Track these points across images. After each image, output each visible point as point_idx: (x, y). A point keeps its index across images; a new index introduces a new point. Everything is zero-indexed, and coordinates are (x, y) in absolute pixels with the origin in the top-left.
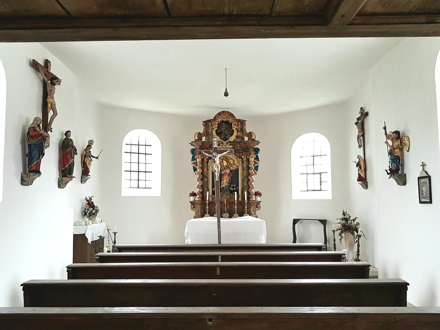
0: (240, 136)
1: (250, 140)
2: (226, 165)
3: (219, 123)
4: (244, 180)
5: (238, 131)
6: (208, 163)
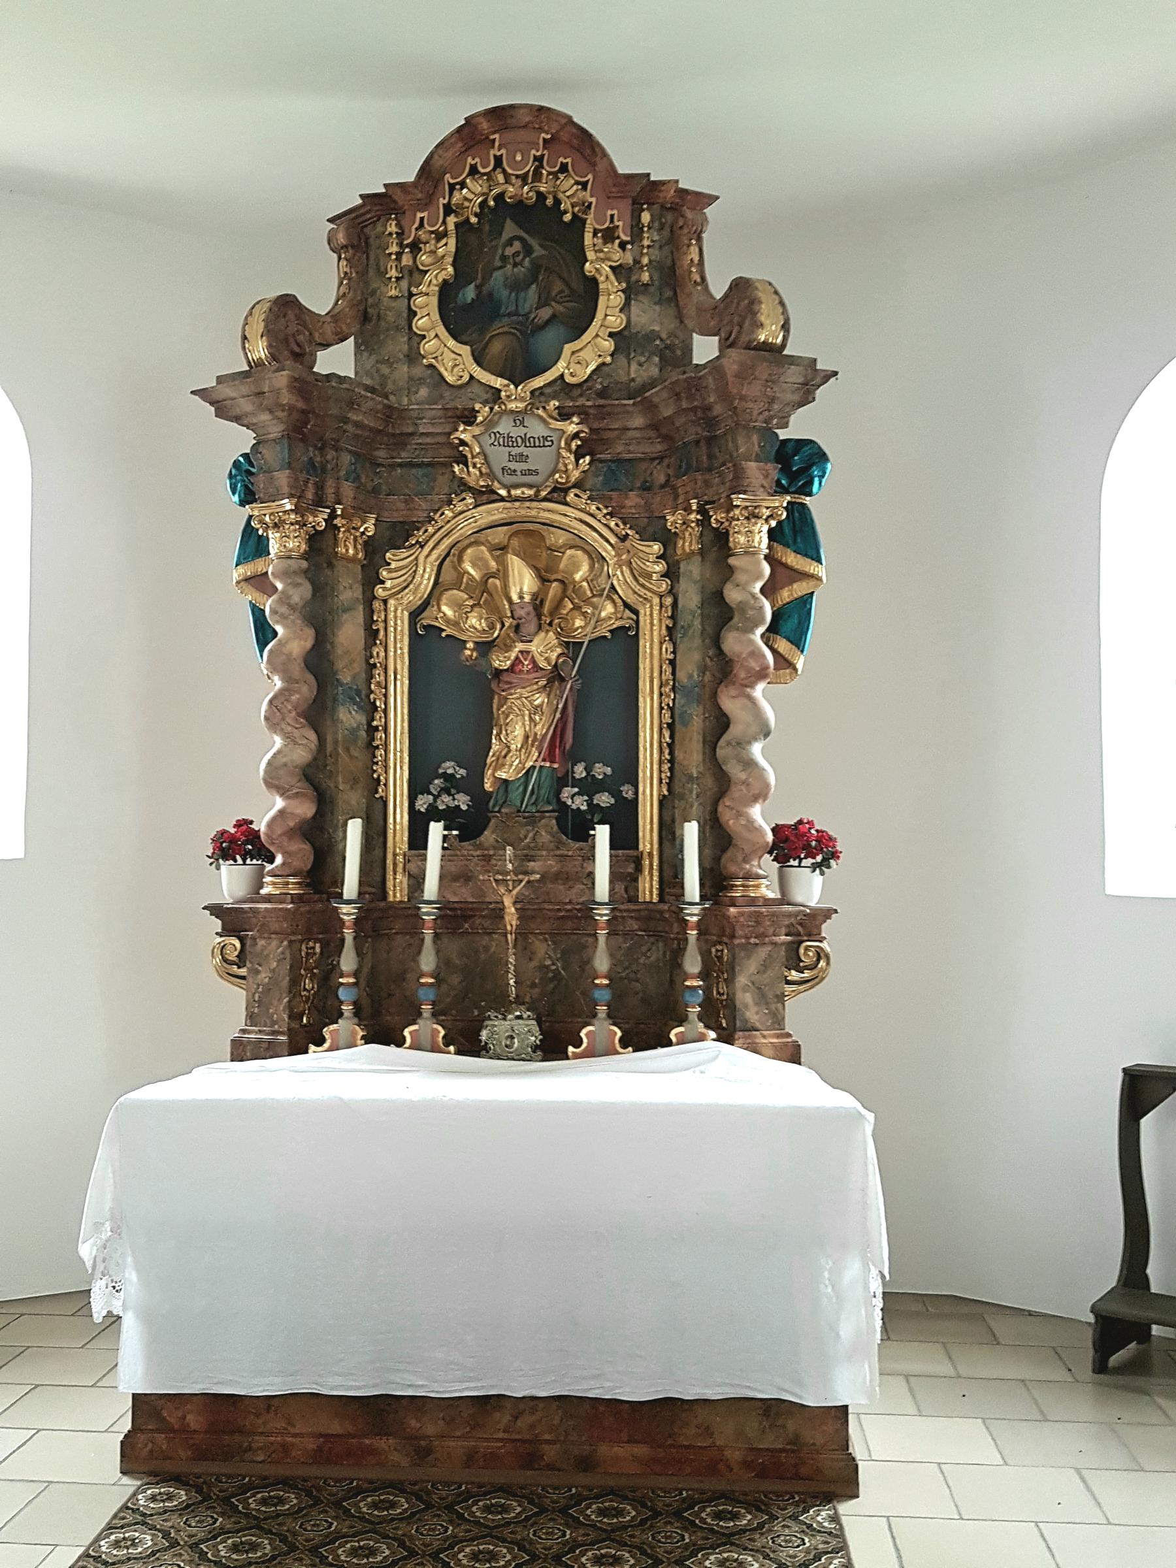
0: (651, 336)
1: (733, 353)
2: (527, 598)
3: (474, 220)
4: (678, 727)
5: (630, 293)
6: (371, 580)
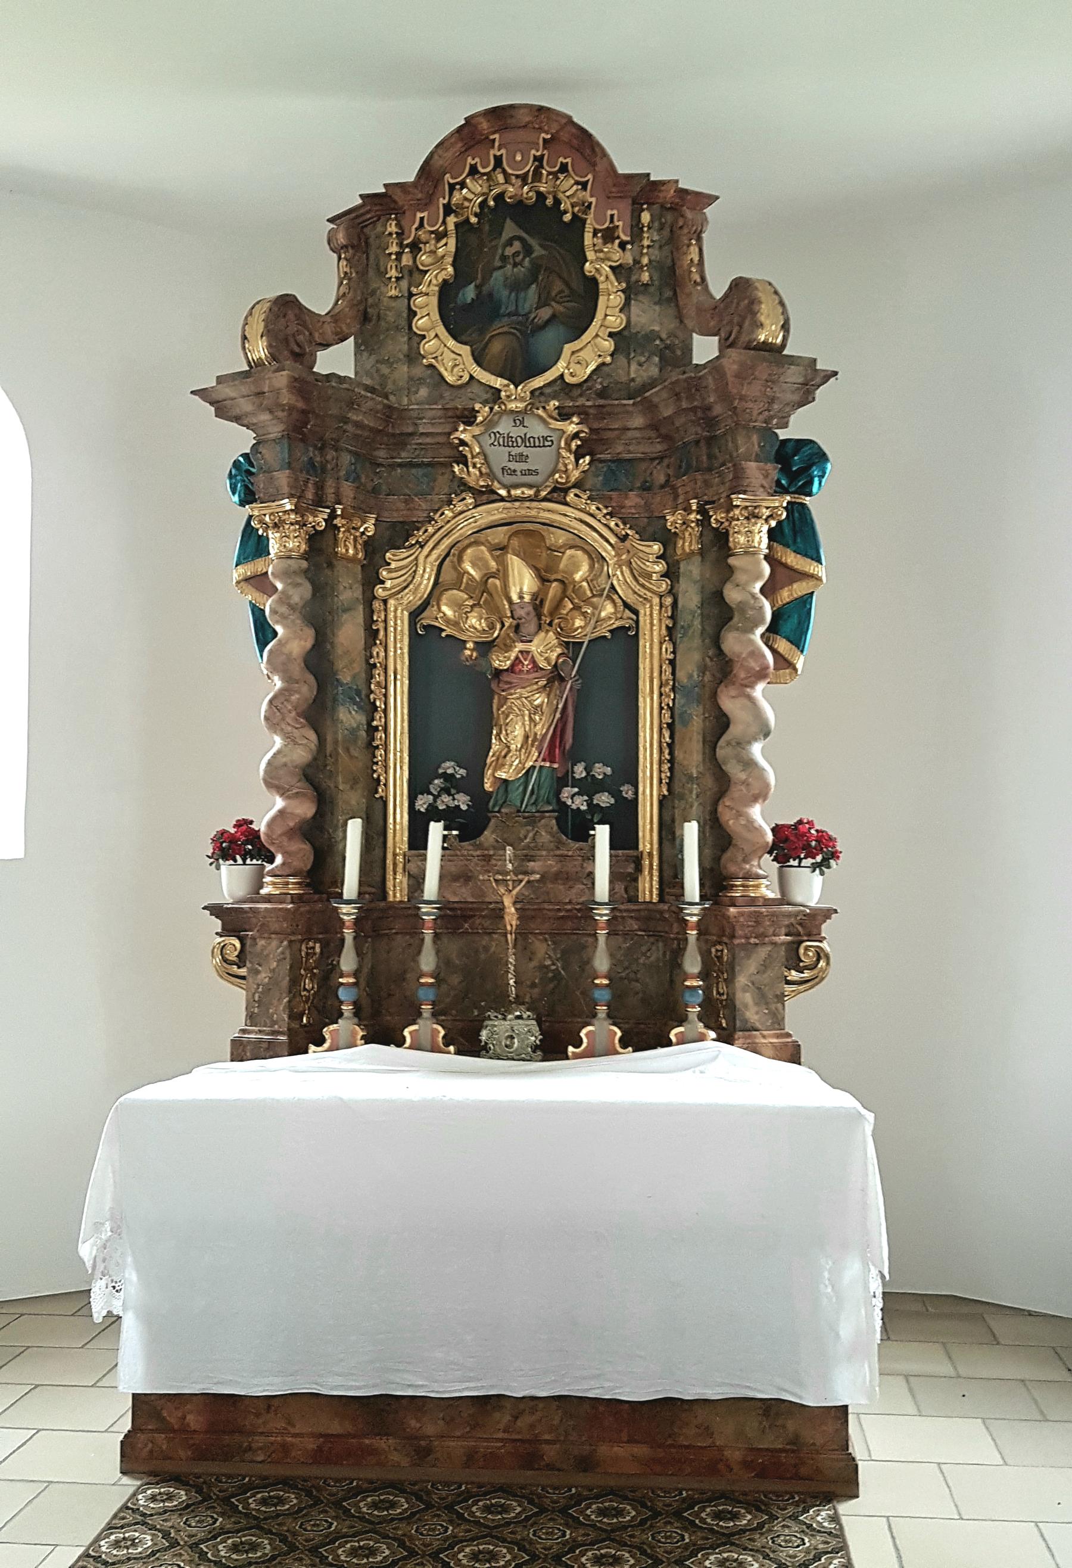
0: (651, 336)
1: (733, 353)
2: (527, 598)
3: (474, 220)
6: (371, 579)
